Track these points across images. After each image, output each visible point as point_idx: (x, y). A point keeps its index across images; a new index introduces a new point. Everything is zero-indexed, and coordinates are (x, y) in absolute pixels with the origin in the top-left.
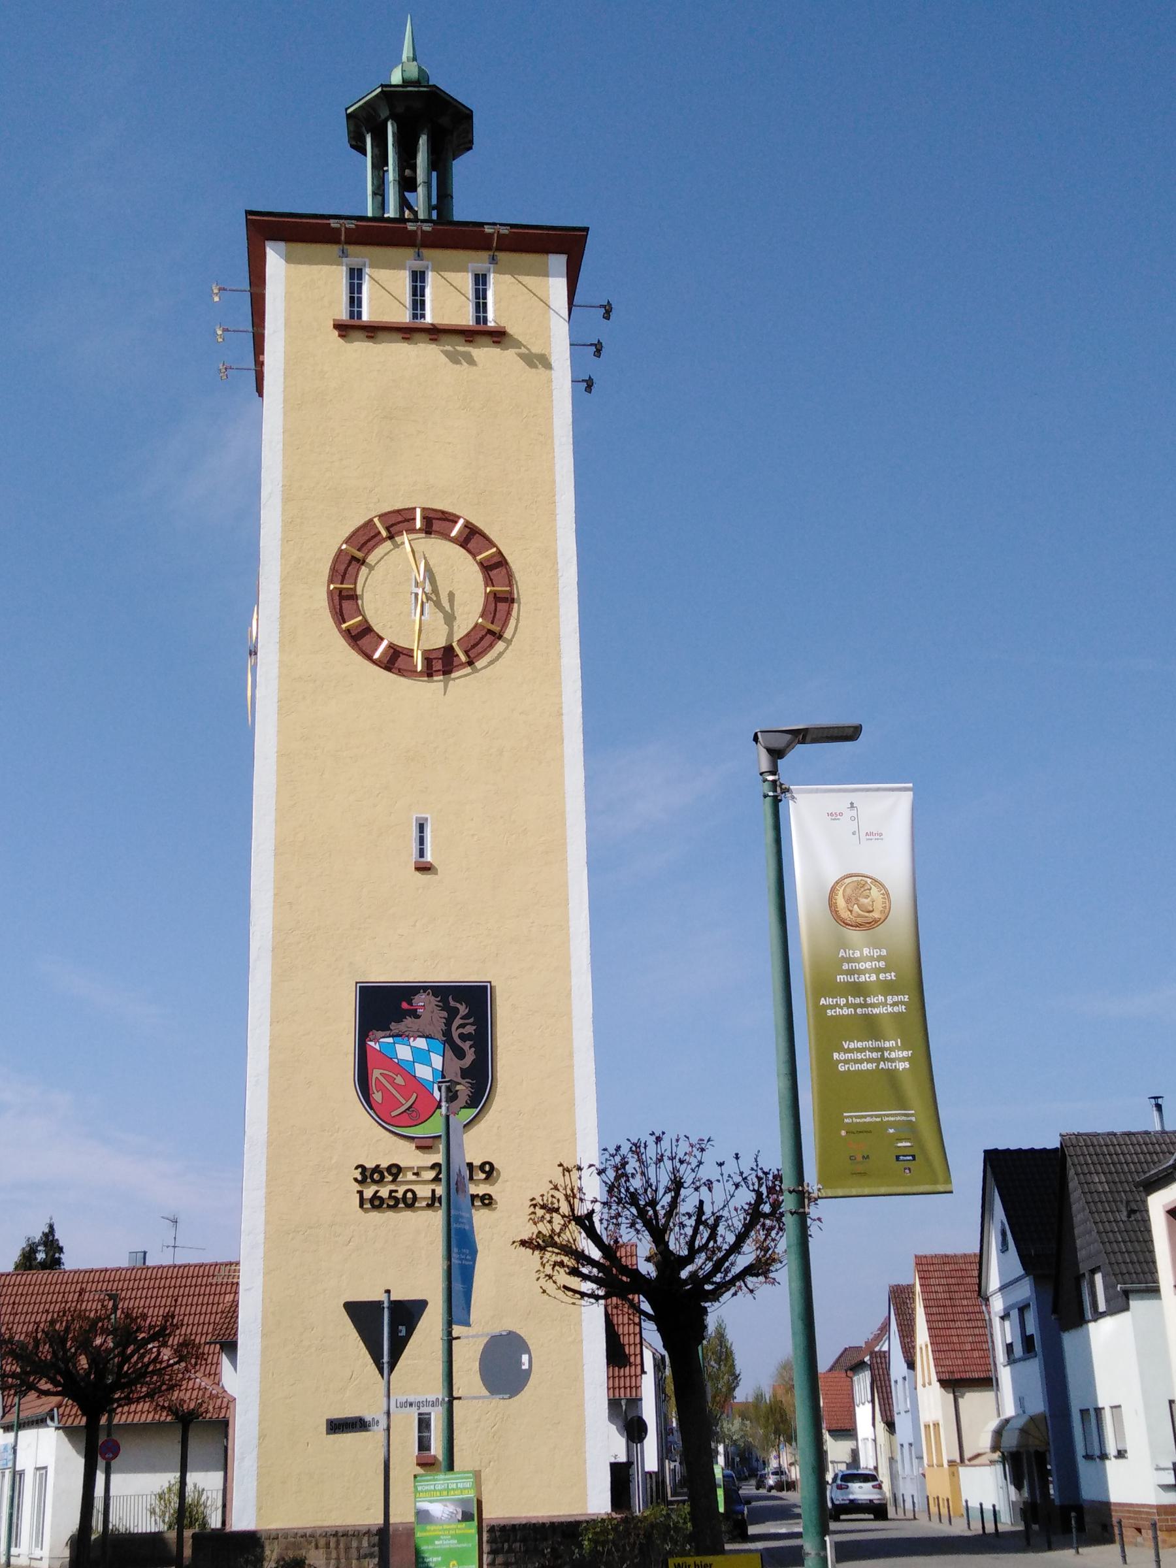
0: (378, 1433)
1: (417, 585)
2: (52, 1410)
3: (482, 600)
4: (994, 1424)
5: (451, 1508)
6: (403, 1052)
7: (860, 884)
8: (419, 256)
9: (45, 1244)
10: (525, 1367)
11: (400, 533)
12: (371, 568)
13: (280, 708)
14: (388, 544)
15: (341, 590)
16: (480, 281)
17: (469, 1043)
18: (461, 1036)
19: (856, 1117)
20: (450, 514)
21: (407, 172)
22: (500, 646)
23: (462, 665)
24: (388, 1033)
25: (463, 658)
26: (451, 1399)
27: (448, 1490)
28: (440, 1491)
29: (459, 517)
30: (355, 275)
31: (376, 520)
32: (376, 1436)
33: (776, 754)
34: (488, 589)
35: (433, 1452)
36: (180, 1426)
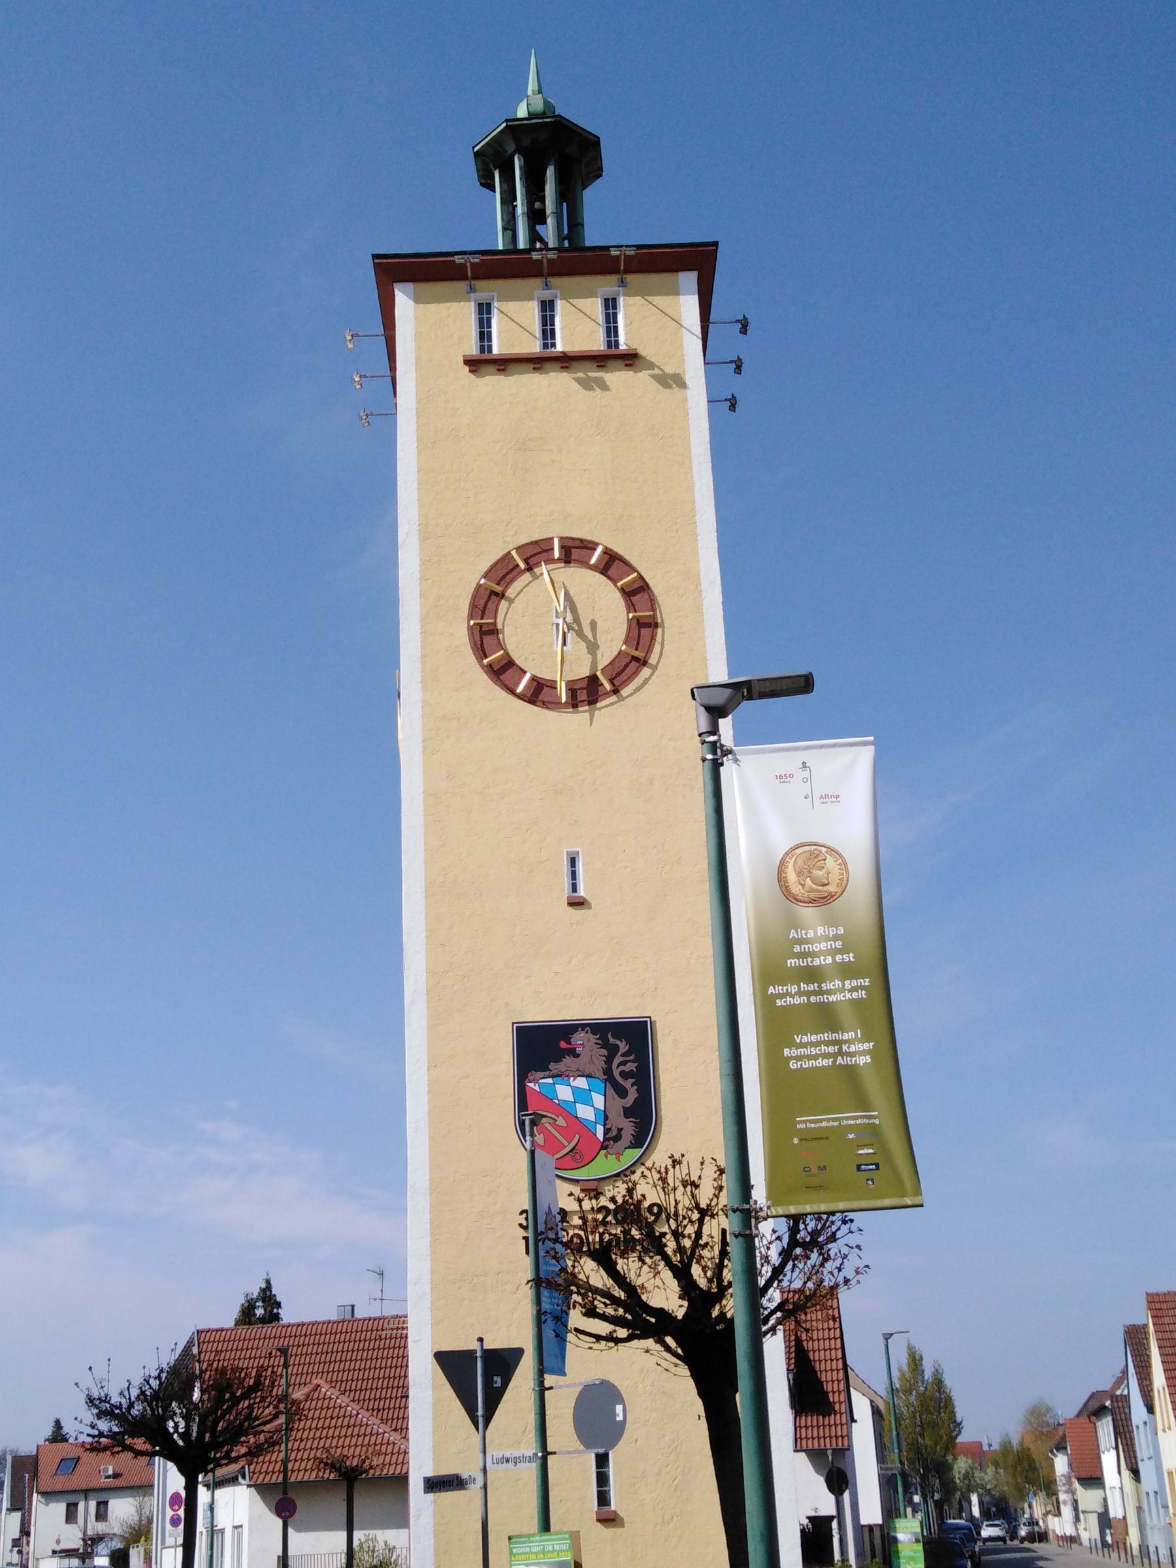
1: (557, 617)
2: (243, 1467)
3: (624, 627)
6: (564, 1093)
7: (813, 854)
8: (547, 286)
10: (620, 1418)
11: (538, 564)
12: (511, 601)
13: (425, 749)
14: (527, 577)
15: (481, 626)
16: (610, 305)
17: (630, 1081)
18: (622, 1074)
19: (811, 1122)
21: (537, 205)
22: (645, 672)
23: (607, 694)
24: (547, 1073)
25: (608, 687)
27: (544, 1552)
28: (536, 1553)
30: (484, 310)
31: (514, 553)
33: (716, 712)
34: (631, 615)
35: (613, 1507)
36: (345, 1483)
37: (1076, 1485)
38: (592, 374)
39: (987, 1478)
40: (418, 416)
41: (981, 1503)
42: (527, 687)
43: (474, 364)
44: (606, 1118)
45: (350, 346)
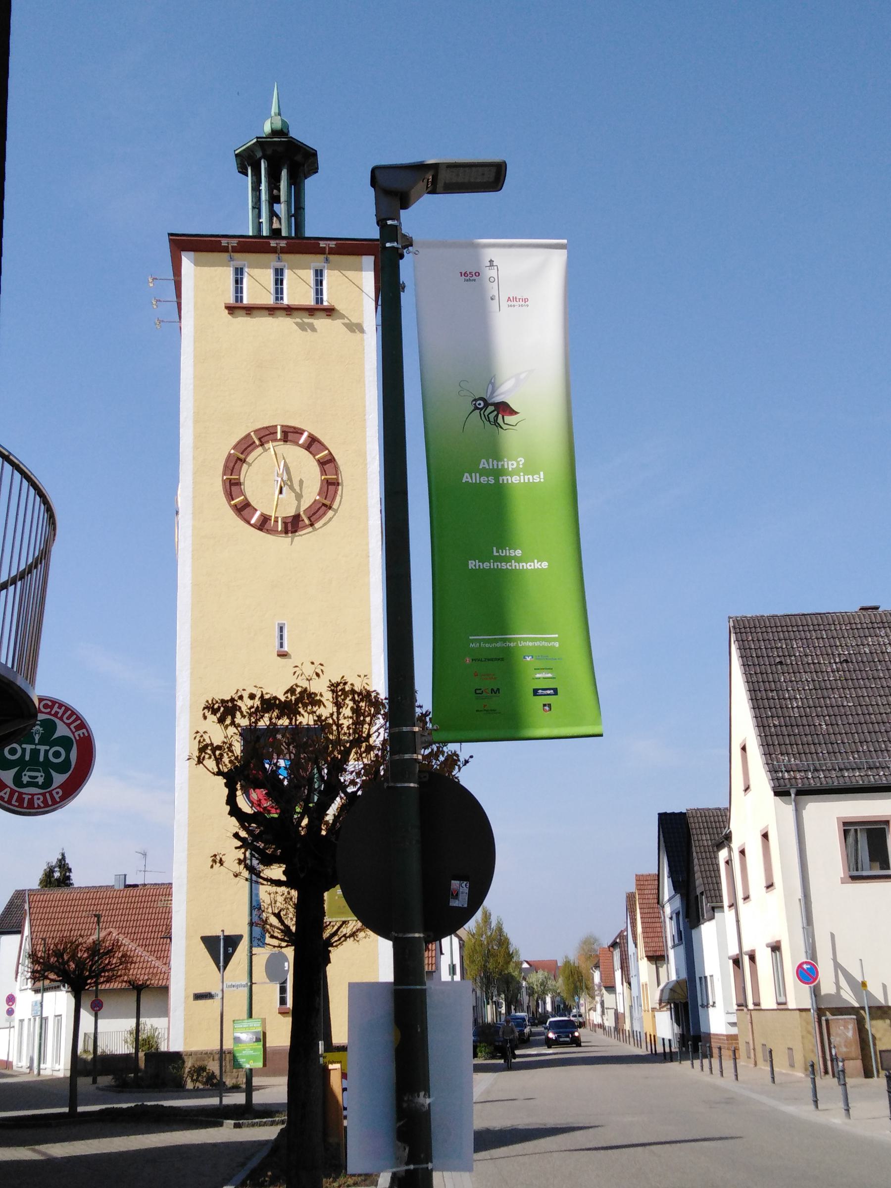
0: (217, 1000)
5: (251, 1036)
9: (60, 867)
11: (268, 442)
12: (250, 465)
14: (260, 449)
15: (230, 480)
16: (319, 273)
20: (300, 429)
22: (330, 513)
23: (306, 527)
25: (307, 522)
26: (252, 983)
29: (304, 431)
30: (239, 272)
31: (252, 434)
32: (216, 1002)
36: (135, 994)
37: (604, 991)
38: (306, 320)
39: (558, 985)
40: (195, 342)
41: (553, 1002)
42: (258, 520)
43: (231, 309)
45: (151, 285)
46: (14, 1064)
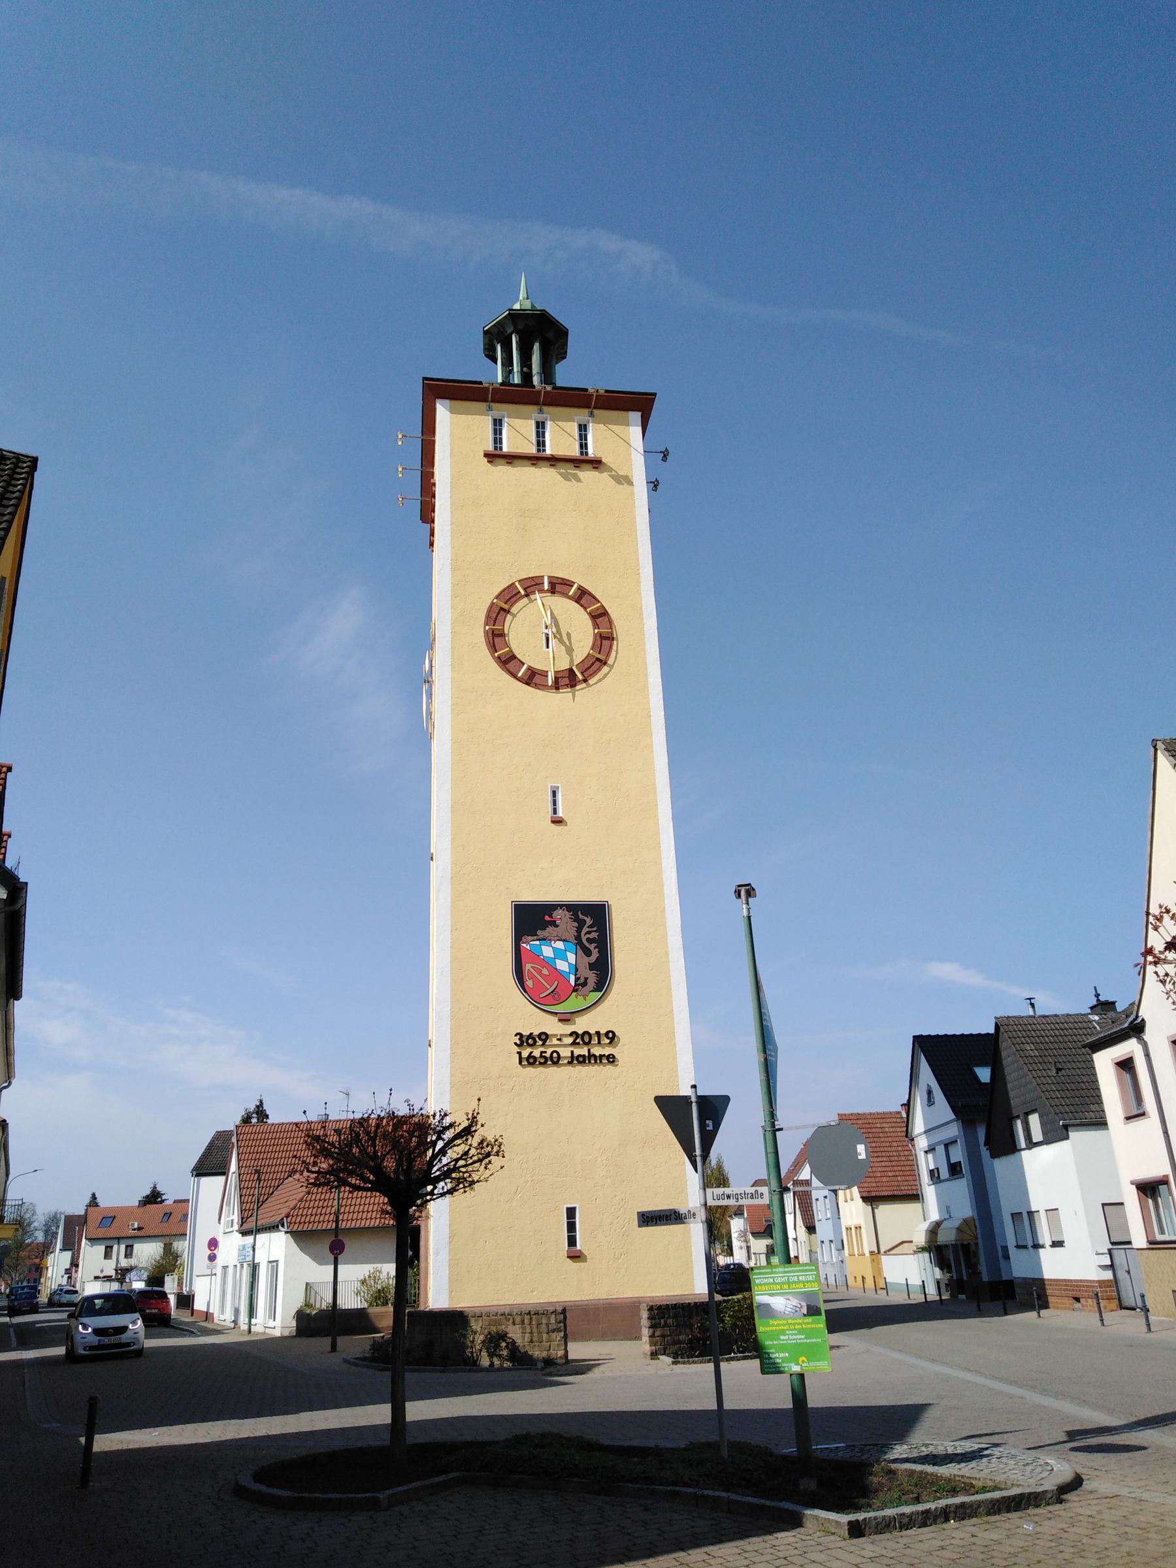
4: (925, 1226)
5: (795, 1302)
6: (547, 951)
9: (257, 1113)
11: (533, 593)
12: (514, 616)
13: (453, 710)
14: (525, 600)
16: (583, 428)
17: (594, 945)
18: (588, 939)
21: (525, 369)
22: (605, 669)
25: (580, 677)
30: (498, 424)
35: (578, 1247)
42: (524, 673)
44: (577, 970)
46: (215, 1316)
